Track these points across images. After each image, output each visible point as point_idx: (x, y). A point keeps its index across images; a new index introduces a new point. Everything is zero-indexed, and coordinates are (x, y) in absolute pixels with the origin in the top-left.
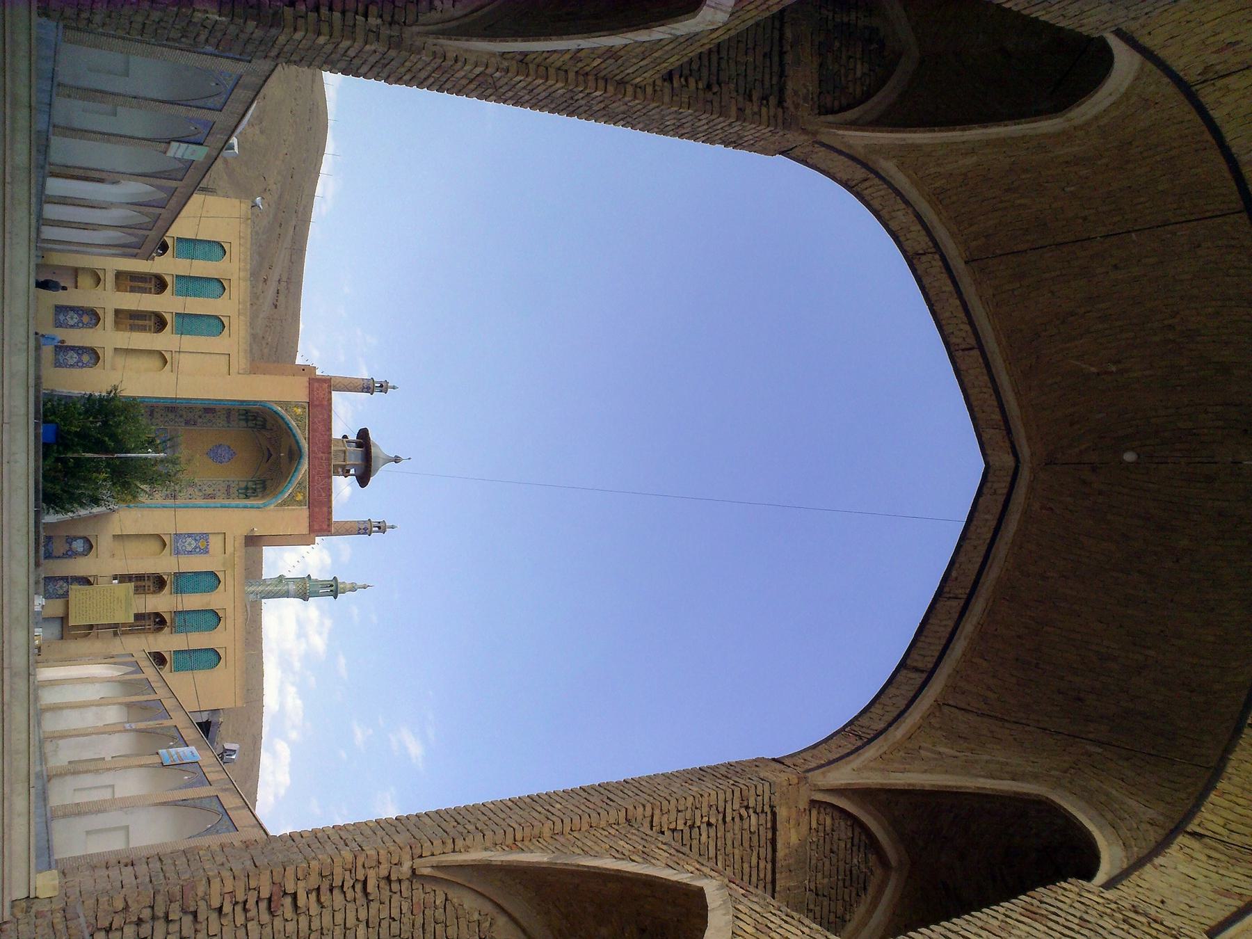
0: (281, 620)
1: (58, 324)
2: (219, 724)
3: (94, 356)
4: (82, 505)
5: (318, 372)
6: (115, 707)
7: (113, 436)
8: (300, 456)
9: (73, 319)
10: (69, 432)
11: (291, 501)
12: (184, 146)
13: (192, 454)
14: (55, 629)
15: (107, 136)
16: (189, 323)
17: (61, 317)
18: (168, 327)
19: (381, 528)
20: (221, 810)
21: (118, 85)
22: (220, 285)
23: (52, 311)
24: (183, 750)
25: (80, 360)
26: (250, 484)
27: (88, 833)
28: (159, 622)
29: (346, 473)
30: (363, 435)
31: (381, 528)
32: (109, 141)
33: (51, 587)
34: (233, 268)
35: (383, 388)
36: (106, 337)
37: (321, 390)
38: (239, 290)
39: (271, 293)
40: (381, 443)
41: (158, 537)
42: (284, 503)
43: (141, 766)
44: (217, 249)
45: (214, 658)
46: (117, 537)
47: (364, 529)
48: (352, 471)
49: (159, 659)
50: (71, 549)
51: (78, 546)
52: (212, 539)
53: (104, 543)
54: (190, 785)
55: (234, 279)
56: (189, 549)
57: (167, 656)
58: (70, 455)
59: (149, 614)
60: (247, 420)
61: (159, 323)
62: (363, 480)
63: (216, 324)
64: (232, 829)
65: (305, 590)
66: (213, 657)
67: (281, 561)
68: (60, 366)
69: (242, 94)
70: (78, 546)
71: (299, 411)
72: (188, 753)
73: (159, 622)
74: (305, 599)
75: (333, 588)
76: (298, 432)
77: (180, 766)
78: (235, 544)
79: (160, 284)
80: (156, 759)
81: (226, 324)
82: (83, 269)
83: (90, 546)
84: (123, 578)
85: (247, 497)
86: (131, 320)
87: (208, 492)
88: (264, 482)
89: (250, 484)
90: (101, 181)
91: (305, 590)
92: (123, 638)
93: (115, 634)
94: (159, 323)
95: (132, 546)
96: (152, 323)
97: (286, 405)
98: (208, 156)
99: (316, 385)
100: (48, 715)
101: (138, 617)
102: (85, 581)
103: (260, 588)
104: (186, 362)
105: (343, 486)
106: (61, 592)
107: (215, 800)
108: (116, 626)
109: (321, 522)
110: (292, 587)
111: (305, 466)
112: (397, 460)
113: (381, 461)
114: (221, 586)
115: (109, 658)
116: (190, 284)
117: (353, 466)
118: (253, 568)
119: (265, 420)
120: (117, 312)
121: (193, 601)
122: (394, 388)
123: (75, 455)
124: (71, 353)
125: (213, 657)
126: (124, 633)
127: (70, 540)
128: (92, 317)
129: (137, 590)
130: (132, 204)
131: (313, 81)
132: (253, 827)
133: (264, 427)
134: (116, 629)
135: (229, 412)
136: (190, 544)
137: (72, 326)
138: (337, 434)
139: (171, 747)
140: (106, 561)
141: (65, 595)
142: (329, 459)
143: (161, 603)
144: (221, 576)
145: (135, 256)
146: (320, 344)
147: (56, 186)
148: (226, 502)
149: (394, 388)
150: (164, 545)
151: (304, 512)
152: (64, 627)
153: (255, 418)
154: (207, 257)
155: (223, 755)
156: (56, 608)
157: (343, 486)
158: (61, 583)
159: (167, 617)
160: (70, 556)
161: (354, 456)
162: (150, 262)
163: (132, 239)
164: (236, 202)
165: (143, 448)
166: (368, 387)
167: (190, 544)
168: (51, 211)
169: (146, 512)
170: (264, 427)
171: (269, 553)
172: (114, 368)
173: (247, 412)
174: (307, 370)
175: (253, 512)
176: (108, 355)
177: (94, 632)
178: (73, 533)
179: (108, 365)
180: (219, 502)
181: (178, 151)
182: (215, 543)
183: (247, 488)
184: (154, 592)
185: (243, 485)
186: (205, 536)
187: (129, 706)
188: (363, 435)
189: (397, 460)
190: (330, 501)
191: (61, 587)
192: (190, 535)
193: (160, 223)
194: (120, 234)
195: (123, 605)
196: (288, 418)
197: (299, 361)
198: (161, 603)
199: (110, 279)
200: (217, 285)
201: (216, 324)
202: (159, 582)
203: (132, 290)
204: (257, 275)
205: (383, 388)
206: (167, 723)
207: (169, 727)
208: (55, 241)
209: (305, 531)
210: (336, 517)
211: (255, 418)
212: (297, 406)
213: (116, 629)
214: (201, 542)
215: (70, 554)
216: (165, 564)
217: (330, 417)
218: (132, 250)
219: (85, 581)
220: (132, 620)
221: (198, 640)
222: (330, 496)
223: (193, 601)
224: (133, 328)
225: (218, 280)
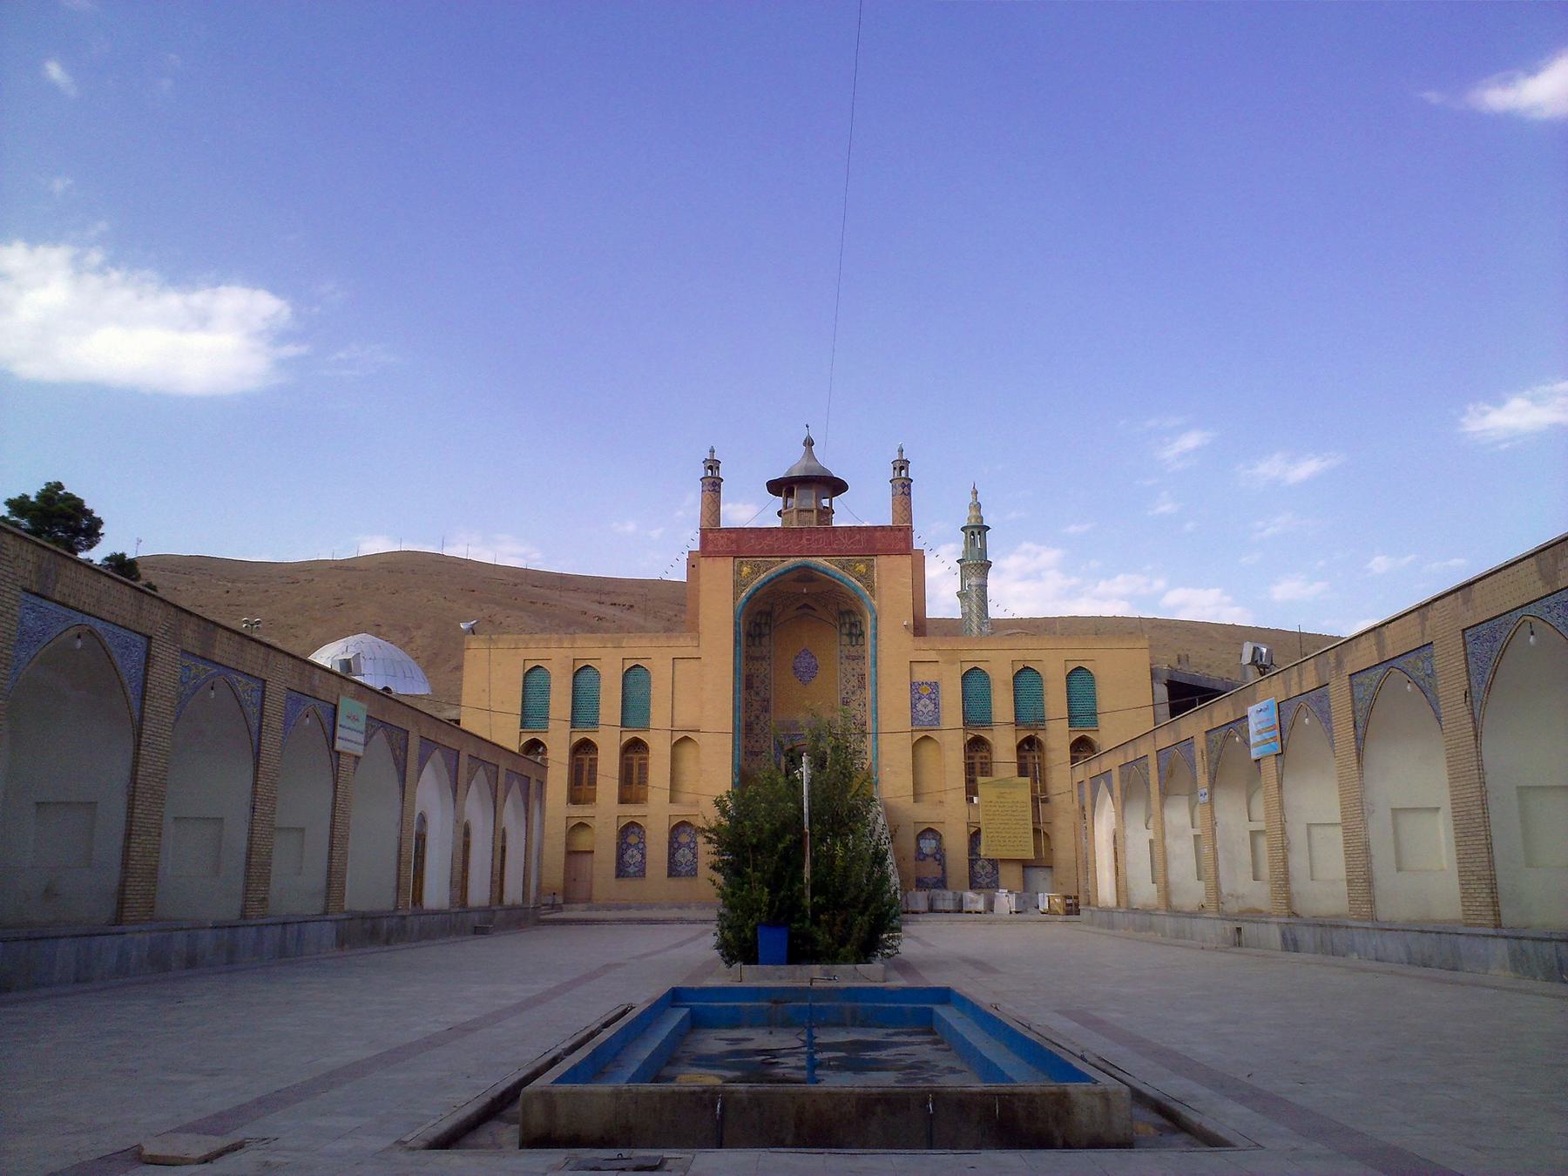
0: (1012, 597)
2: (1172, 670)
3: (679, 828)
4: (885, 878)
5: (696, 547)
6: (1166, 812)
7: (777, 836)
8: (806, 568)
9: (633, 856)
10: (771, 904)
11: (866, 578)
12: (340, 732)
13: (809, 706)
14: (1039, 876)
15: (336, 839)
16: (634, 707)
17: (631, 870)
19: (902, 465)
20: (1381, 670)
21: (237, 836)
22: (582, 674)
23: (626, 882)
24: (1254, 724)
26: (845, 631)
27: (1399, 870)
28: (1029, 747)
29: (827, 513)
30: (775, 487)
31: (902, 465)
32: (345, 837)
33: (984, 881)
34: (558, 657)
35: (713, 465)
36: (657, 813)
37: (719, 541)
38: (589, 648)
39: (610, 611)
40: (788, 463)
42: (870, 587)
43: (1280, 786)
44: (534, 679)
46: (917, 796)
47: (903, 487)
48: (826, 502)
49: (1082, 748)
50: (933, 856)
51: (928, 846)
52: (918, 678)
53: (925, 813)
54: (1325, 717)
55: (572, 654)
56: (931, 707)
58: (807, 902)
59: (1019, 757)
60: (761, 635)
61: (635, 747)
62: (838, 487)
63: (634, 677)
64: (1426, 652)
65: (976, 565)
66: (1079, 678)
67: (943, 595)
69: (223, 650)
70: (928, 846)
71: (746, 570)
72: (1259, 717)
73: (1029, 747)
74: (989, 565)
75: (977, 531)
77: (1284, 729)
78: (926, 649)
79: (583, 750)
80: (1270, 767)
83: (929, 832)
84: (971, 790)
85: (862, 634)
86: (632, 783)
88: (841, 613)
89: (845, 631)
90: (421, 839)
91: (976, 565)
92: (1053, 791)
93: (1045, 801)
94: (635, 747)
95: (930, 780)
96: (636, 756)
97: (738, 585)
98: (358, 697)
99: (710, 548)
100: (1175, 901)
101: (1022, 771)
102: (975, 837)
103: (975, 619)
104: (685, 718)
105: (847, 512)
106: (989, 868)
107: (1357, 680)
108: (1035, 800)
109: (896, 540)
110: (974, 581)
111: (821, 562)
112: (809, 443)
113: (812, 463)
114: (981, 666)
115: (1085, 815)
116: (583, 709)
117: (818, 501)
118: (948, 628)
119: (760, 613)
120: (623, 800)
121: (1002, 705)
122: (712, 451)
123: (808, 893)
124: (678, 857)
125: (1079, 678)
126: (1044, 790)
127: (920, 856)
128: (629, 832)
129: (987, 772)
130: (455, 792)
131: (354, 569)
132: (1424, 619)
133: (769, 614)
134: (1040, 800)
135: (750, 658)
136: (925, 705)
137: (643, 856)
138: (777, 523)
139: (1246, 742)
140: (949, 811)
141: (994, 863)
142: (810, 530)
143: (1004, 744)
144: (967, 667)
145: (542, 784)
146: (650, 542)
147: (436, 894)
148: (869, 660)
149: (712, 451)
151: (881, 562)
152: (1038, 863)
153: (758, 625)
154: (546, 690)
155: (1262, 667)
156: (1010, 875)
157: (847, 512)
158: (977, 868)
160: (943, 856)
161: (805, 499)
163: (516, 787)
164: (468, 655)
165: (795, 785)
166: (713, 485)
167: (925, 705)
168: (479, 894)
169: (883, 761)
170: (769, 614)
171: (931, 613)
173: (749, 635)
174: (692, 565)
176: (680, 811)
178: (912, 853)
180: (868, 670)
181: (350, 738)
182: (924, 674)
183: (850, 635)
185: (846, 639)
186: (915, 687)
187: (1165, 793)
188: (775, 487)
189: (809, 443)
191: (982, 869)
192: (913, 706)
193: (484, 756)
194: (509, 803)
195: (1006, 793)
197: (679, 574)
198: (1004, 744)
199: (579, 811)
200: (582, 675)
201: (634, 677)
202: (976, 746)
203: (593, 782)
204: (593, 625)
205: (713, 465)
206: (1200, 744)
207: (1208, 741)
208: (526, 884)
209: (907, 560)
210: (887, 521)
212: (739, 572)
213: (1040, 800)
214: (923, 694)
215: (939, 855)
216: (952, 744)
218: (533, 791)
219: (975, 837)
220: (1027, 780)
221: (1055, 701)
223: (1002, 705)
224: (643, 780)
225: (576, 675)
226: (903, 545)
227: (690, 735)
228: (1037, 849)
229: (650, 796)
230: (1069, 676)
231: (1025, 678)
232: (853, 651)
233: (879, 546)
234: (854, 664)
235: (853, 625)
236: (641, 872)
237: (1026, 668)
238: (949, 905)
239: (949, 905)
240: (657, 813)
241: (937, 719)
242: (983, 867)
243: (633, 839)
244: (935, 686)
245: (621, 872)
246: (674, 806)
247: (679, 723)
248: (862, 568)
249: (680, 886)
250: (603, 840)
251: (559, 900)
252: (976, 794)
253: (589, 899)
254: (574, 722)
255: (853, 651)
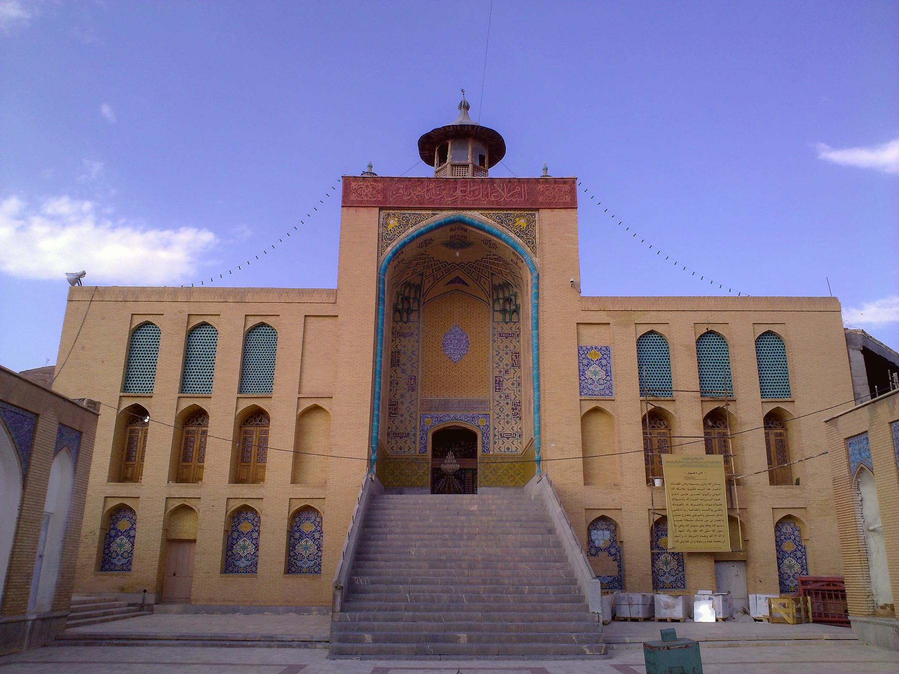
1: (316, 569)
3: (302, 515)
8: (462, 221)
9: (244, 547)
11: (527, 234)
17: (242, 563)
18: (261, 404)
25: (311, 535)
26: (498, 307)
28: (716, 419)
33: (668, 580)
36: (274, 496)
41: (586, 417)
45: (769, 340)
46: (588, 479)
50: (607, 549)
52: (586, 342)
53: (599, 498)
56: (602, 374)
57: (770, 407)
60: (409, 311)
61: (253, 419)
68: (130, 562)
70: (601, 537)
71: (393, 223)
76: (423, 225)
81: (258, 320)
82: (166, 530)
83: (603, 521)
84: (653, 471)
85: (516, 311)
86: (247, 463)
87: (508, 360)
89: (498, 307)
94: (253, 419)
97: (383, 241)
99: (353, 197)
102: (659, 526)
104: (315, 383)
106: (674, 564)
108: (729, 482)
111: (476, 216)
114: (659, 329)
121: (684, 371)
122: (370, 166)
128: (241, 517)
135: (396, 334)
136: (595, 372)
141: (679, 557)
142: (465, 181)
143: (688, 416)
150: (596, 410)
151: (544, 216)
153: (406, 299)
159: (710, 407)
160: (619, 550)
162: (102, 410)
169: (547, 435)
170: (418, 288)
172: (324, 484)
173: (396, 310)
175: (545, 283)
176: (303, 493)
177: (736, 514)
179: (318, 493)
182: (593, 338)
183: (504, 311)
184: (668, 427)
185: (499, 316)
186: (582, 351)
190: (528, 181)
191: (666, 565)
192: (582, 373)
195: (691, 468)
196: (403, 237)
198: (688, 416)
199: (182, 491)
202: (655, 419)
211: (406, 299)
212: (385, 225)
216: (628, 407)
217: (401, 180)
219: (659, 526)
222: (520, 181)
223: (684, 371)
225: (190, 333)
226: (568, 198)
227: (320, 403)
228: (733, 541)
229: (268, 475)
230: (759, 340)
231: (709, 341)
232: (507, 329)
233: (541, 199)
234: (506, 342)
235: (508, 300)
236: (252, 569)
237: (710, 332)
238: (638, 611)
239: (638, 611)
240: (274, 496)
241: (610, 388)
242: (667, 563)
243: (246, 527)
244: (605, 352)
245: (229, 565)
246: (782, 490)
247: (307, 390)
248: (522, 222)
249: (298, 584)
250: (208, 530)
251: (151, 599)
252: (660, 475)
253: (188, 600)
254: (183, 387)
255: (507, 329)
